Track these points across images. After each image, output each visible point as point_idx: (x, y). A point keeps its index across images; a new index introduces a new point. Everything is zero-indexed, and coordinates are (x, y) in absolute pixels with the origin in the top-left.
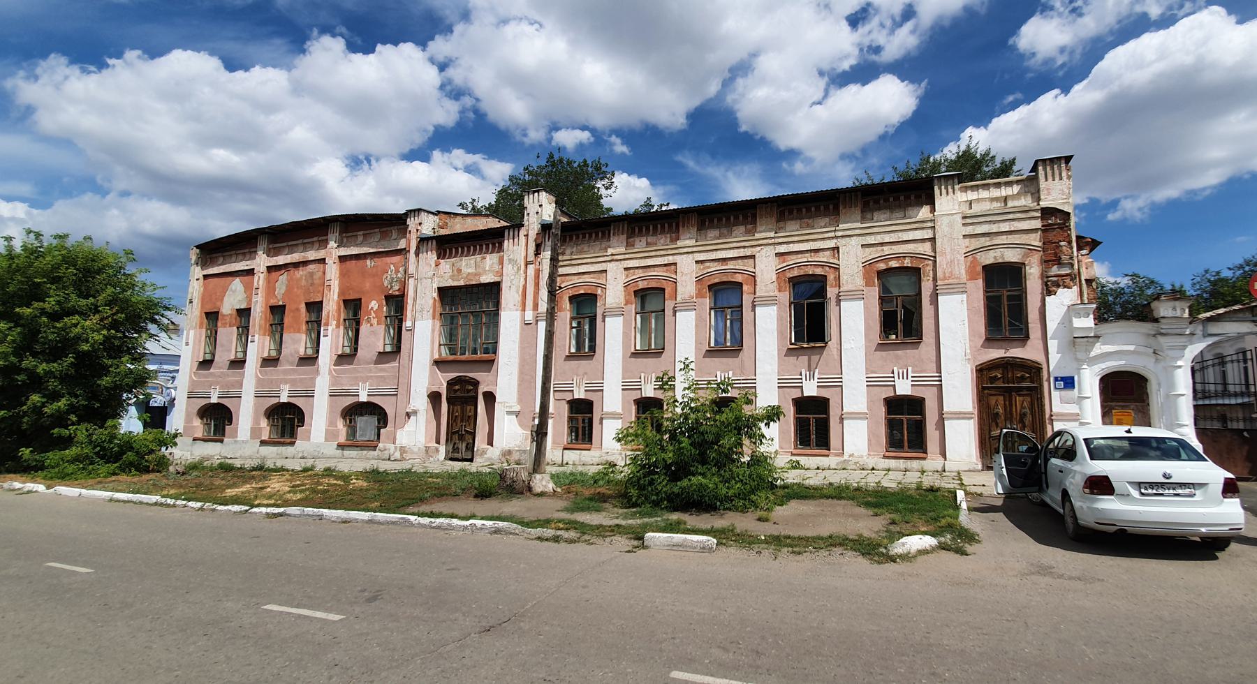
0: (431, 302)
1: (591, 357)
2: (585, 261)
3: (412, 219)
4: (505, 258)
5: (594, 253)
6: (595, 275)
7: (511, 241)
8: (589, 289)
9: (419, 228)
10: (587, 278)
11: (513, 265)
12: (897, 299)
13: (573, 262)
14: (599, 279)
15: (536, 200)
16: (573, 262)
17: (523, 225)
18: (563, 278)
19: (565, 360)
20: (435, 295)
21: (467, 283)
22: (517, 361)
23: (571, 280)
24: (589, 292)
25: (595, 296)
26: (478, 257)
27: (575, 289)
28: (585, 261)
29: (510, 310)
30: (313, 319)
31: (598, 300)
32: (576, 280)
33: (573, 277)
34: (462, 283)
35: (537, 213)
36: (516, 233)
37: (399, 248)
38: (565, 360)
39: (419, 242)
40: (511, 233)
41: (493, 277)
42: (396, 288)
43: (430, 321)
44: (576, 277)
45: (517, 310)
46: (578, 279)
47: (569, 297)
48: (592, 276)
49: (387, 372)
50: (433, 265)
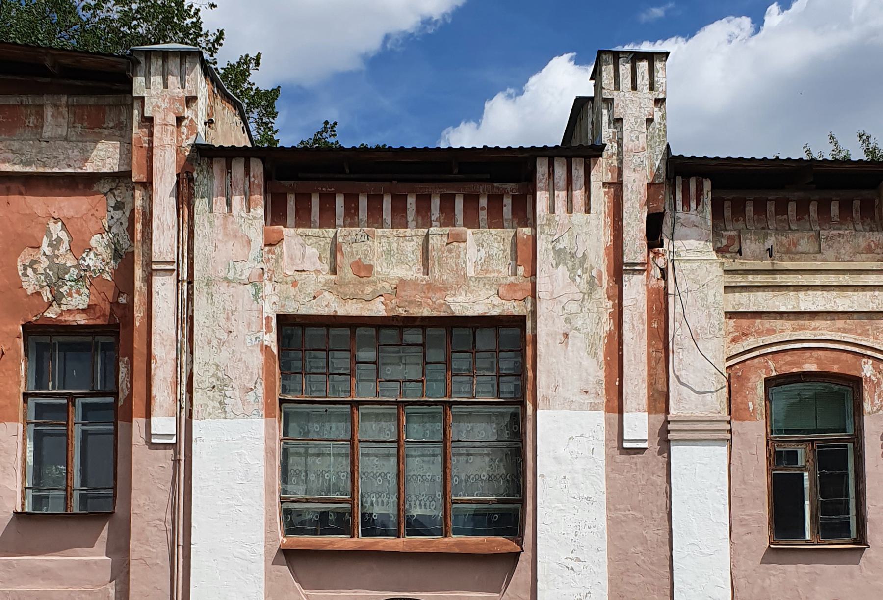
0: (257, 360)
1: (858, 553)
2: (819, 280)
3: (157, 80)
4: (542, 245)
5: (837, 260)
6: (850, 323)
7: (561, 195)
8: (835, 361)
9: (188, 113)
10: (824, 330)
11: (572, 270)
12: (455, 502)
13: (780, 279)
14: (865, 333)
15: (643, 81)
16: (780, 279)
17: (597, 150)
18: (745, 323)
19: (764, 561)
20: (271, 339)
21: (401, 312)
22: (603, 557)
23: (771, 331)
24: (835, 369)
25: (857, 382)
26: (438, 234)
27: (788, 358)
28: (819, 280)
29: (570, 404)
30: (443, 378)
31: (866, 395)
32: (787, 331)
33: (778, 324)
34: (378, 309)
35: (649, 121)
36: (578, 172)
37: (89, 168)
38: (764, 561)
39: (189, 160)
40: (560, 172)
41: (496, 300)
42: (80, 301)
43: (262, 422)
44: (788, 324)
45: (593, 407)
46: (795, 330)
47: (767, 380)
48: (840, 324)
49: (59, 580)
50: (259, 241)
